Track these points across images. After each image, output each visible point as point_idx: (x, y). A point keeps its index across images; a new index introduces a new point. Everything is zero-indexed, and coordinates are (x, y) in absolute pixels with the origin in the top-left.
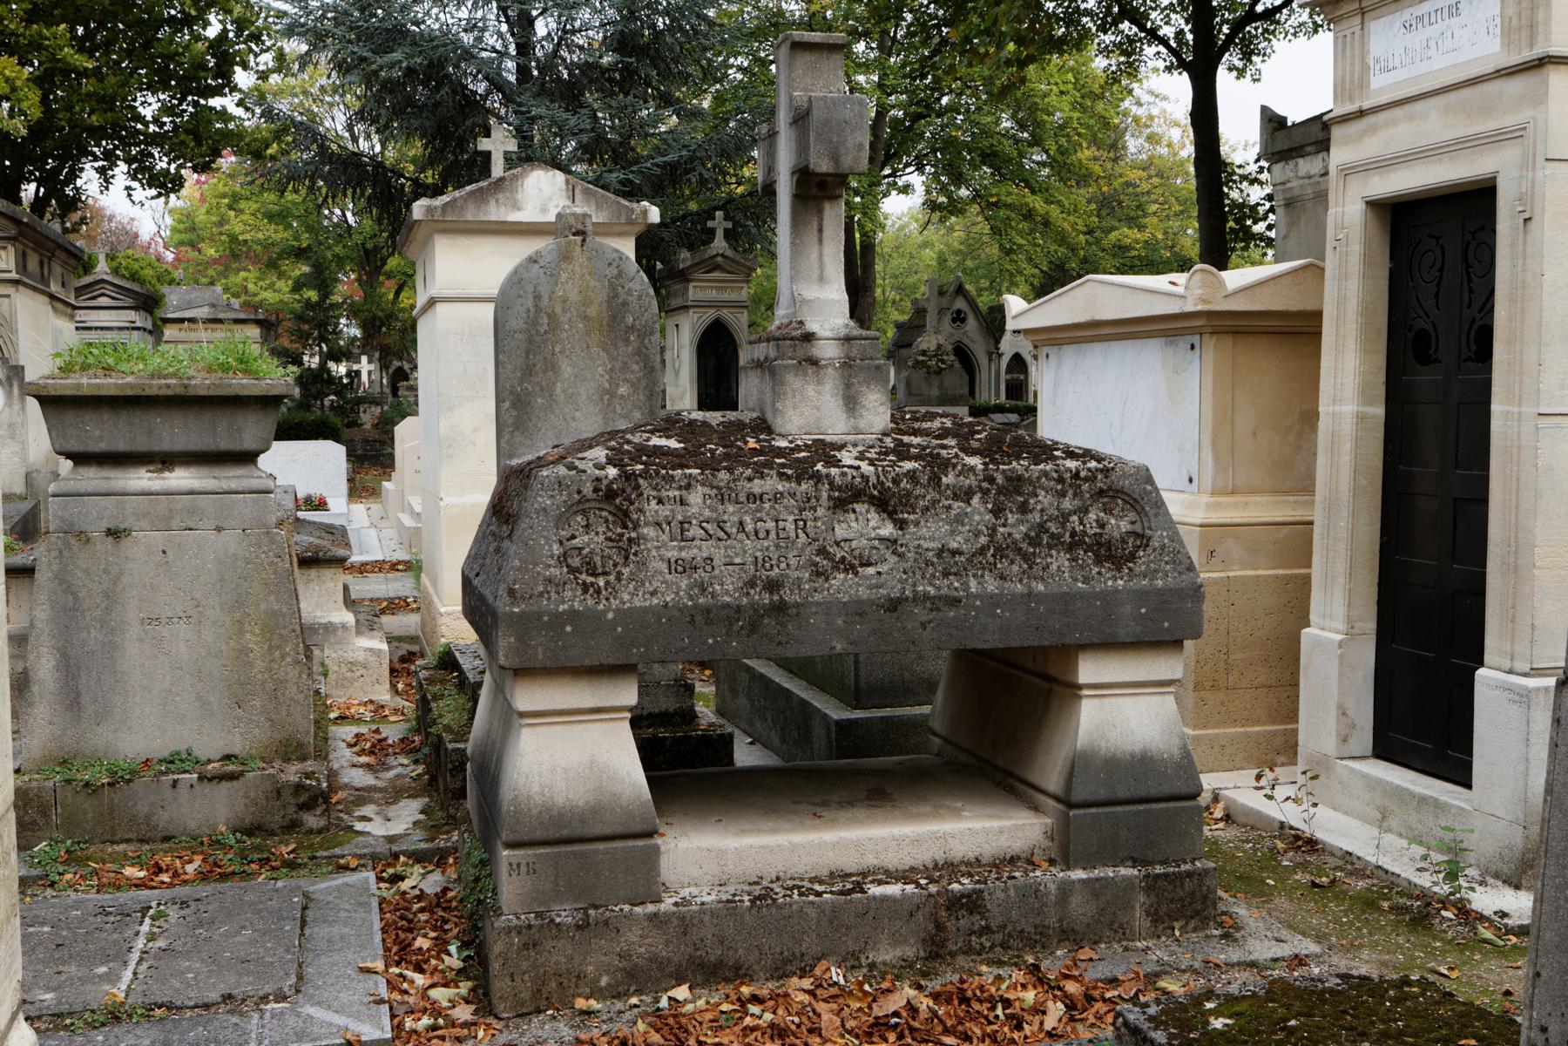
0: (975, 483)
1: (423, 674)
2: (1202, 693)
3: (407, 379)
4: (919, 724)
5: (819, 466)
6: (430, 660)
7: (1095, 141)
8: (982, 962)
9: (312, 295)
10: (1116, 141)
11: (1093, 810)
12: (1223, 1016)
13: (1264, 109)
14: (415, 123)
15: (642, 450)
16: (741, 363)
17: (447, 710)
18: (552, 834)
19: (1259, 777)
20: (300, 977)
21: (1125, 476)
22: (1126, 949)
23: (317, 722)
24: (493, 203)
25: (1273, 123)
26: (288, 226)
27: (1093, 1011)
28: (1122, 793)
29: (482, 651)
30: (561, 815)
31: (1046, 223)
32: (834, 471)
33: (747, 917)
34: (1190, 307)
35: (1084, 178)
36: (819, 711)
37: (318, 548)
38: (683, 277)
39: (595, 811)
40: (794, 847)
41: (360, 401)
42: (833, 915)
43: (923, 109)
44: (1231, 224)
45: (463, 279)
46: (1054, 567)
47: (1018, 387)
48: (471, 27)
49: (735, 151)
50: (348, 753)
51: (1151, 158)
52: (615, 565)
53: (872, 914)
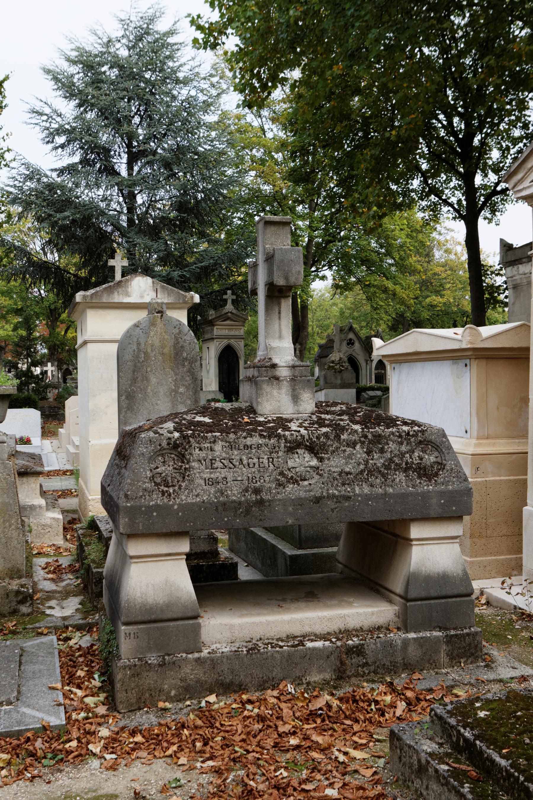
0: (357, 438)
1: (81, 532)
2: (475, 541)
3: (71, 374)
4: (331, 557)
5: (280, 431)
6: (84, 524)
7: (418, 253)
8: (364, 681)
9: (24, 333)
10: (429, 252)
11: (419, 603)
12: (484, 710)
13: (502, 240)
14: (76, 247)
15: (191, 423)
16: (241, 378)
17: (93, 551)
18: (147, 618)
19: (503, 583)
20: (19, 692)
21: (432, 434)
22: (437, 673)
23: (27, 558)
24: (116, 293)
25: (506, 247)
26: (11, 298)
27: (420, 706)
28: (433, 593)
29: (110, 520)
30: (151, 608)
31: (394, 294)
32: (287, 433)
33: (245, 659)
34: (464, 346)
35: (413, 272)
36: (281, 550)
37: (27, 467)
38: (211, 323)
39: (168, 606)
40: (268, 623)
41: (47, 386)
42: (289, 658)
43: (331, 238)
44: (487, 296)
45: (102, 331)
46: (398, 480)
47: (381, 378)
48: (104, 199)
49: (237, 259)
50: (42, 572)
51: (446, 261)
52: (178, 482)
53: (308, 657)
